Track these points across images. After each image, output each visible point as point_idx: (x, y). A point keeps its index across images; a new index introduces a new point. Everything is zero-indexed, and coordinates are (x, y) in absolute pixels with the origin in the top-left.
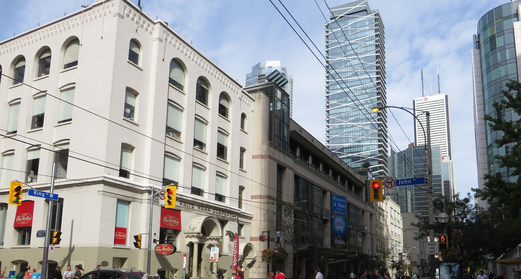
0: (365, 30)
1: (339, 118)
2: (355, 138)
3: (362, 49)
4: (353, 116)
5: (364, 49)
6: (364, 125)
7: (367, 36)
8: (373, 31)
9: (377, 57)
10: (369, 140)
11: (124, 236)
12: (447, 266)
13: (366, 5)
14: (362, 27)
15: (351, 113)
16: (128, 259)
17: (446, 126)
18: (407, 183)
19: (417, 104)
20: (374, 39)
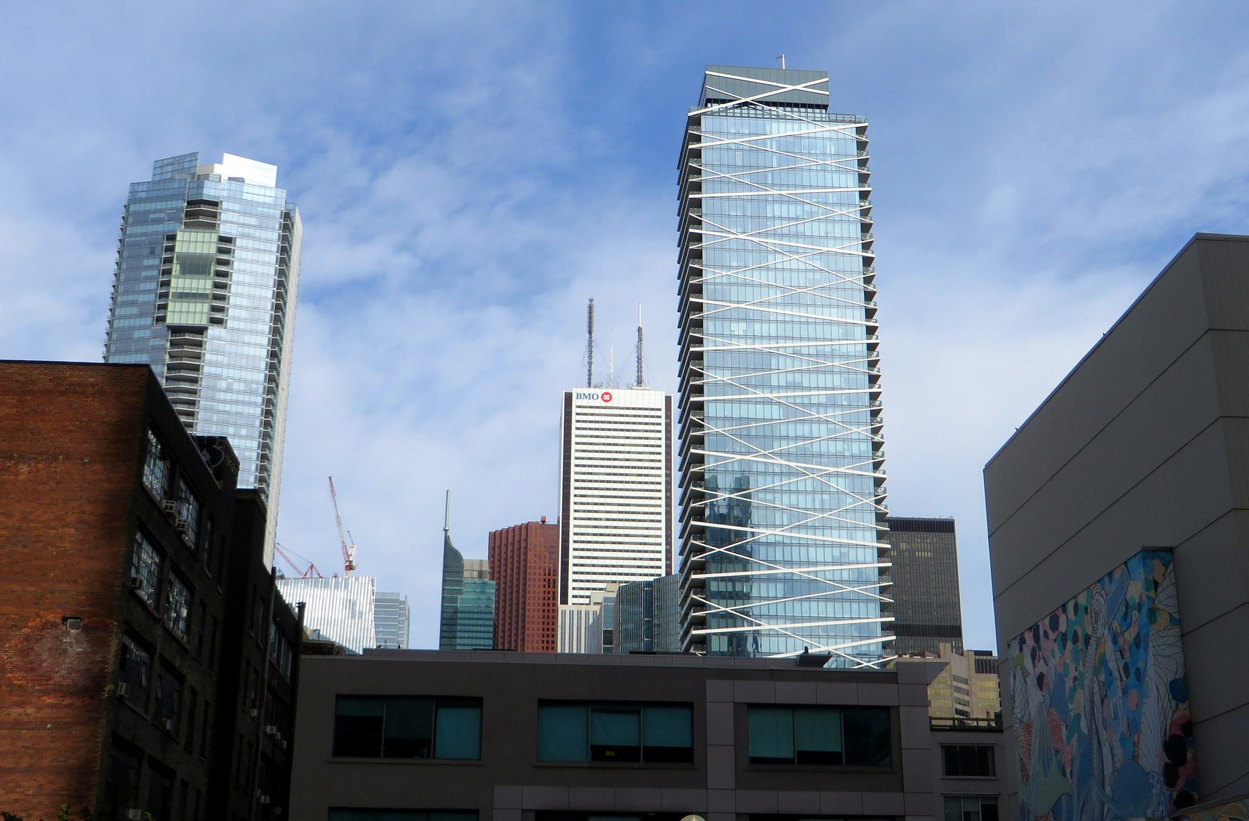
1: (741, 436)
2: (800, 517)
15: (783, 427)
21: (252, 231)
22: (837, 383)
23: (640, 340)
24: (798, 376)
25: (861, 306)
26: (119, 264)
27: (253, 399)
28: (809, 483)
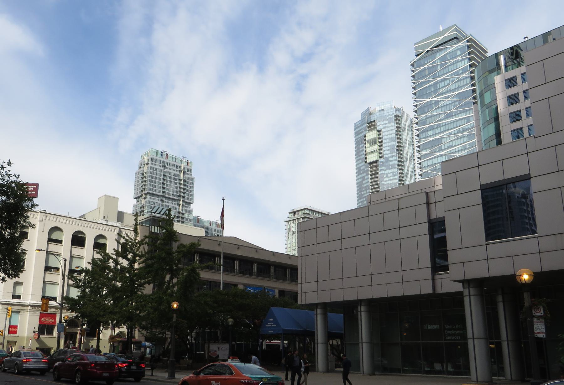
21: (386, 125)
22: (465, 140)
24: (451, 143)
26: (513, 101)
27: (395, 177)
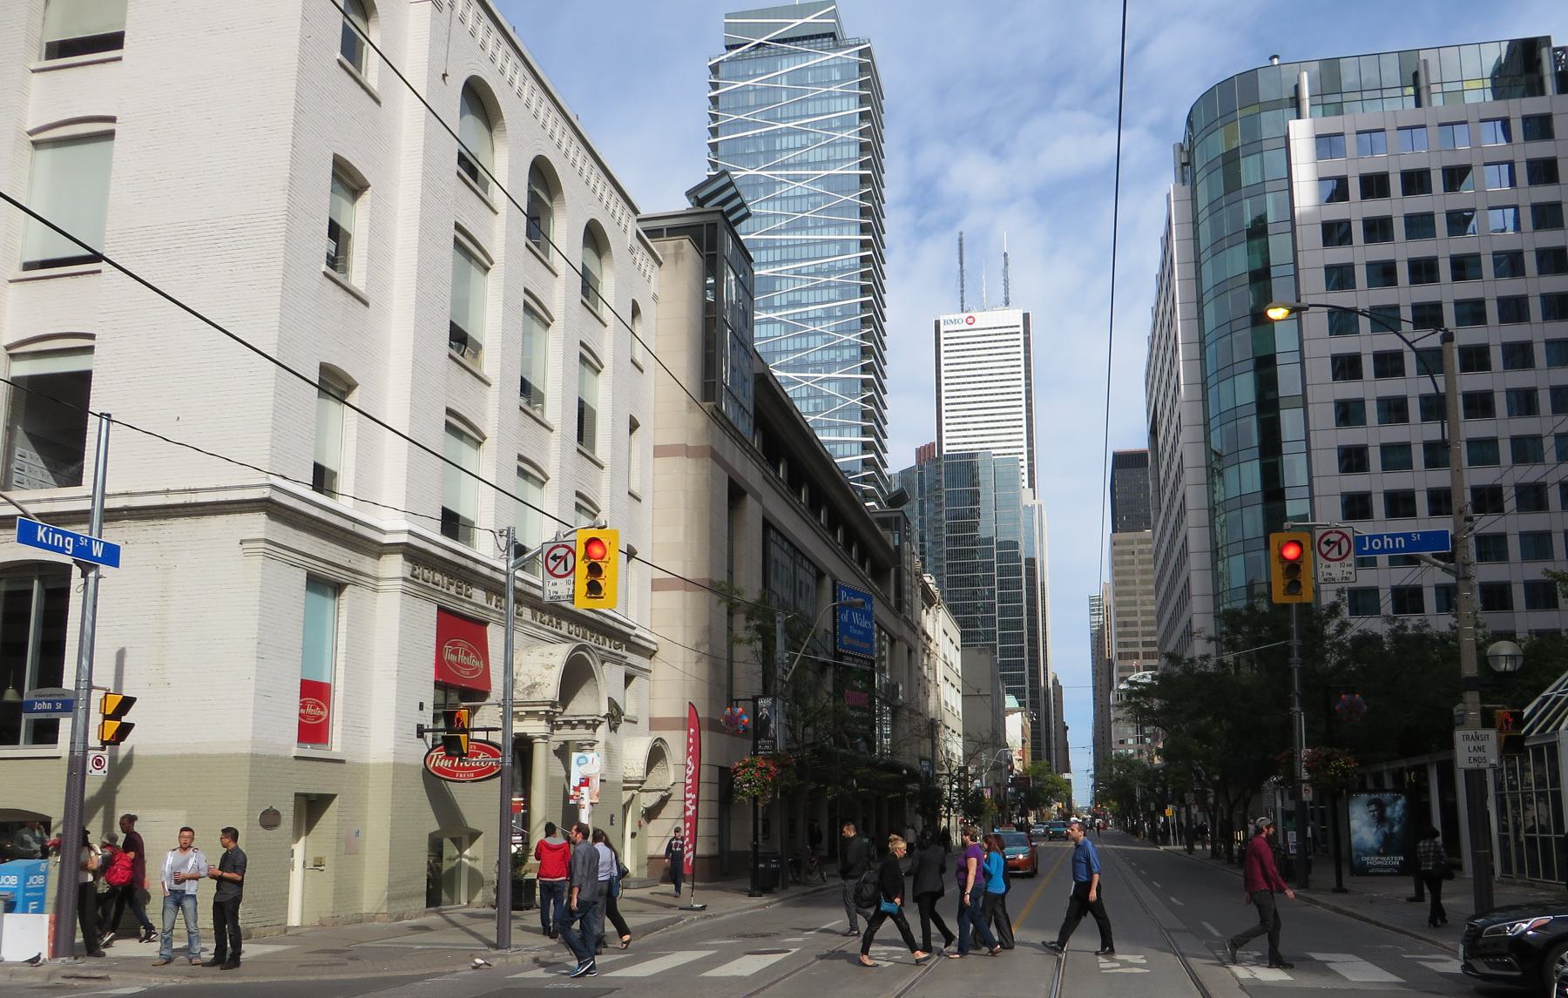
0: (831, 96)
3: (818, 150)
4: (787, 352)
5: (825, 150)
6: (822, 381)
7: (835, 112)
8: (854, 101)
9: (864, 180)
10: (835, 427)
11: (322, 713)
12: (1369, 804)
13: (834, 21)
14: (821, 84)
15: (784, 343)
16: (337, 800)
17: (1023, 402)
18: (1391, 547)
19: (947, 332)
20: (856, 127)
22: (832, 297)
23: (1006, 264)
25: (856, 222)
28: (804, 389)
